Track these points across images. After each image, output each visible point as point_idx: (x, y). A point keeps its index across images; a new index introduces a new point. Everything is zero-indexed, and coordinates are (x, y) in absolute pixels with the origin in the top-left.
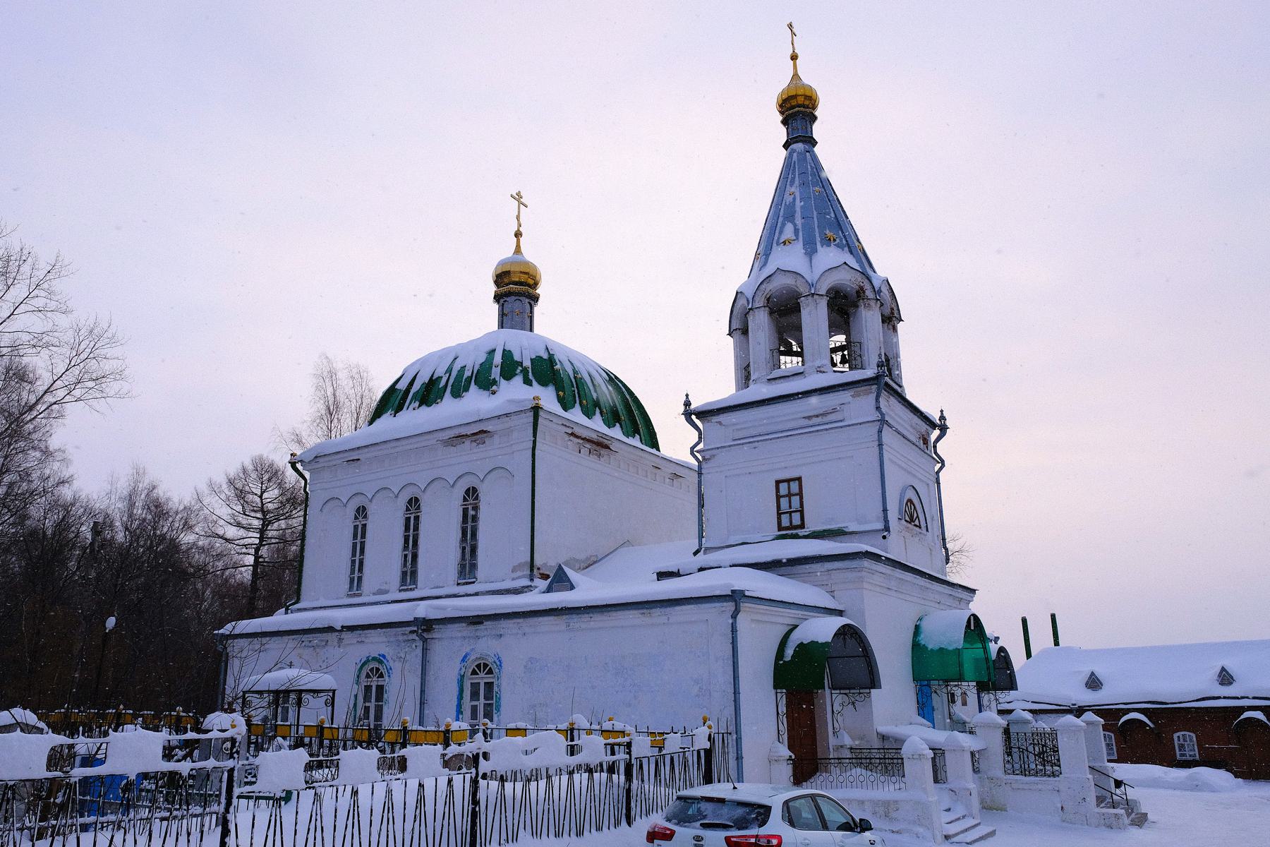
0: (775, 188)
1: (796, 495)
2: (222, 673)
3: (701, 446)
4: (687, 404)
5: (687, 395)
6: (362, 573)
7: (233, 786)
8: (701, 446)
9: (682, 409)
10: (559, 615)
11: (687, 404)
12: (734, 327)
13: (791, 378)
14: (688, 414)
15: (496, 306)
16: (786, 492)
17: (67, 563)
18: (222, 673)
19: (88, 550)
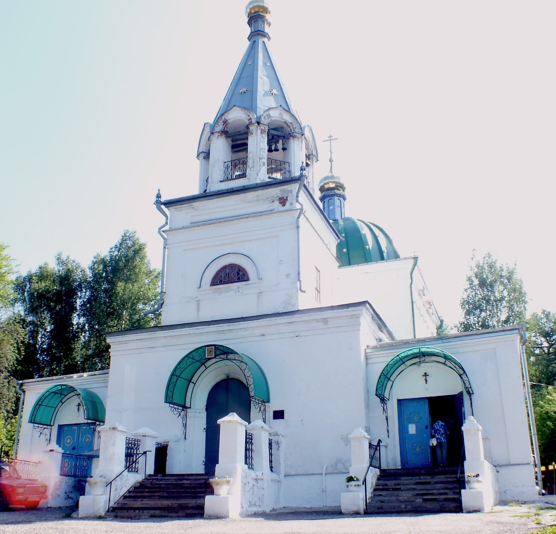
0: (384, 229)
1: (206, 367)
2: (463, 415)
3: (167, 228)
4: (159, 196)
5: (159, 190)
6: (526, 402)
7: (444, 475)
8: (167, 228)
9: (155, 199)
10: (349, 517)
11: (159, 196)
12: (201, 150)
13: (275, 109)
14: (159, 203)
15: (436, 330)
16: (178, 375)
17: (73, 330)
18: (463, 415)
19: (86, 327)
